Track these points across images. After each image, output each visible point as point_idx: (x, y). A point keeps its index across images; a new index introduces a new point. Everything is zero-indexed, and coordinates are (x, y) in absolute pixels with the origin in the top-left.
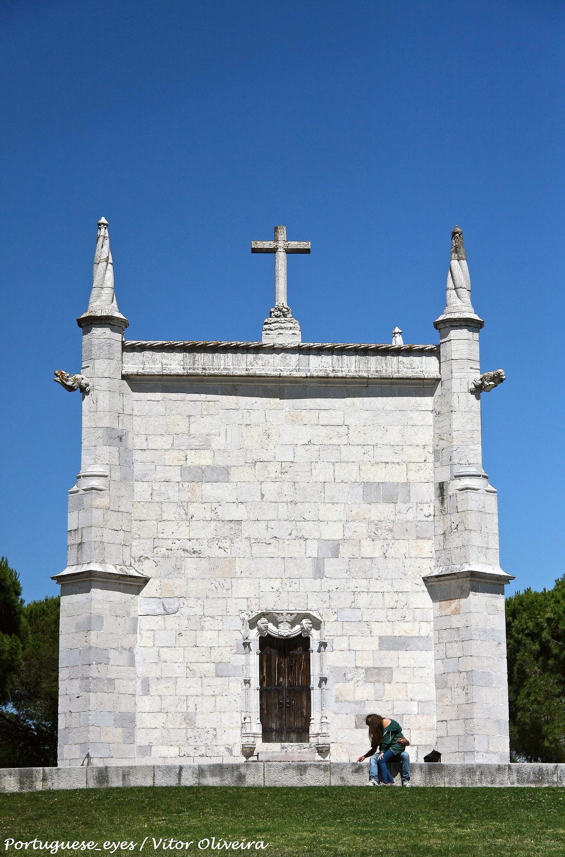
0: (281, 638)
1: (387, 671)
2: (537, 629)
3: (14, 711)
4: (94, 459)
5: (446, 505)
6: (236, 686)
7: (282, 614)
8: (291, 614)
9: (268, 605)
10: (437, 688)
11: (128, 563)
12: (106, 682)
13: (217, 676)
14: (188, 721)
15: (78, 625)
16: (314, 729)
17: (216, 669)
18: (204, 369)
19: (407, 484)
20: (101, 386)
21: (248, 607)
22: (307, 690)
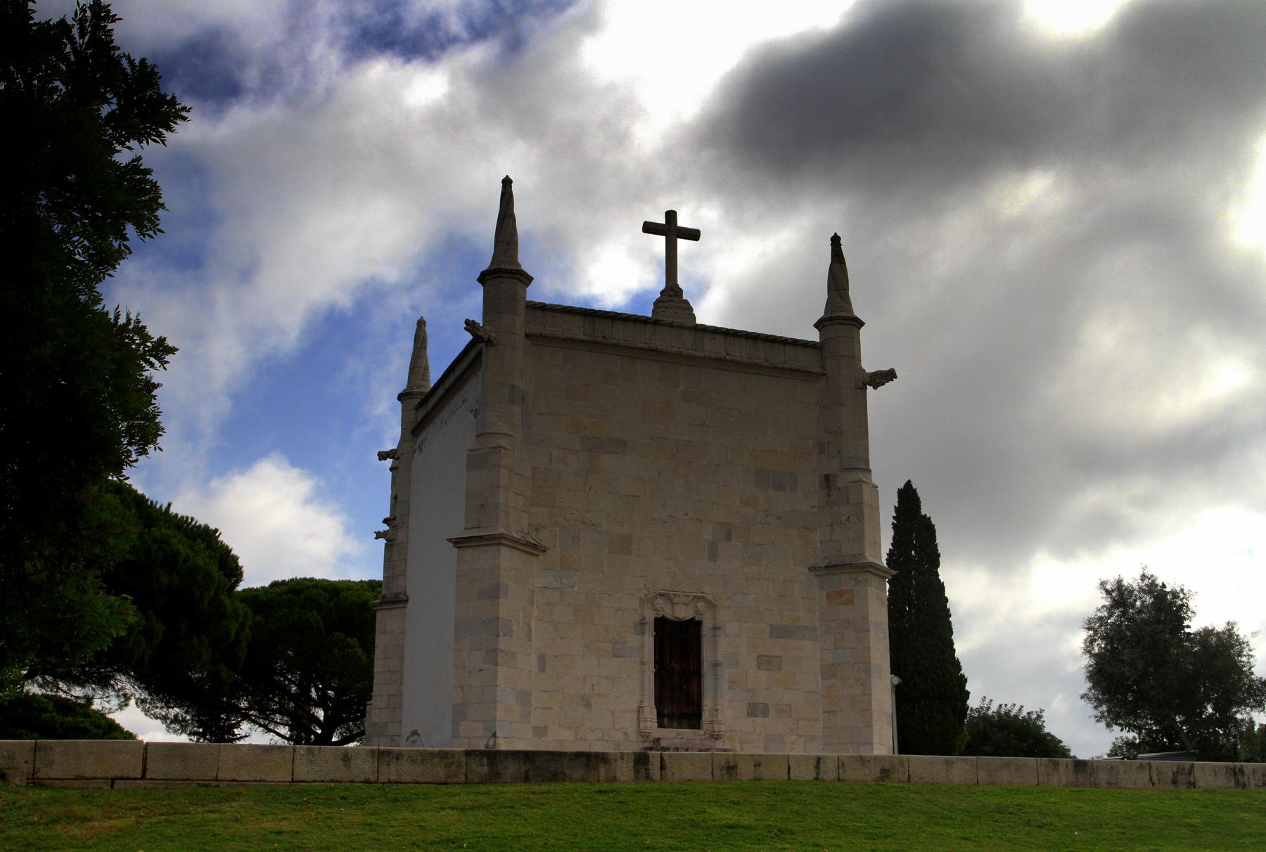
2: (87, 611)
3: (23, 672)
8: (688, 596)
10: (823, 679)
11: (526, 531)
13: (615, 656)
14: (585, 702)
16: (706, 716)
18: (604, 337)
21: (645, 586)
22: (698, 674)
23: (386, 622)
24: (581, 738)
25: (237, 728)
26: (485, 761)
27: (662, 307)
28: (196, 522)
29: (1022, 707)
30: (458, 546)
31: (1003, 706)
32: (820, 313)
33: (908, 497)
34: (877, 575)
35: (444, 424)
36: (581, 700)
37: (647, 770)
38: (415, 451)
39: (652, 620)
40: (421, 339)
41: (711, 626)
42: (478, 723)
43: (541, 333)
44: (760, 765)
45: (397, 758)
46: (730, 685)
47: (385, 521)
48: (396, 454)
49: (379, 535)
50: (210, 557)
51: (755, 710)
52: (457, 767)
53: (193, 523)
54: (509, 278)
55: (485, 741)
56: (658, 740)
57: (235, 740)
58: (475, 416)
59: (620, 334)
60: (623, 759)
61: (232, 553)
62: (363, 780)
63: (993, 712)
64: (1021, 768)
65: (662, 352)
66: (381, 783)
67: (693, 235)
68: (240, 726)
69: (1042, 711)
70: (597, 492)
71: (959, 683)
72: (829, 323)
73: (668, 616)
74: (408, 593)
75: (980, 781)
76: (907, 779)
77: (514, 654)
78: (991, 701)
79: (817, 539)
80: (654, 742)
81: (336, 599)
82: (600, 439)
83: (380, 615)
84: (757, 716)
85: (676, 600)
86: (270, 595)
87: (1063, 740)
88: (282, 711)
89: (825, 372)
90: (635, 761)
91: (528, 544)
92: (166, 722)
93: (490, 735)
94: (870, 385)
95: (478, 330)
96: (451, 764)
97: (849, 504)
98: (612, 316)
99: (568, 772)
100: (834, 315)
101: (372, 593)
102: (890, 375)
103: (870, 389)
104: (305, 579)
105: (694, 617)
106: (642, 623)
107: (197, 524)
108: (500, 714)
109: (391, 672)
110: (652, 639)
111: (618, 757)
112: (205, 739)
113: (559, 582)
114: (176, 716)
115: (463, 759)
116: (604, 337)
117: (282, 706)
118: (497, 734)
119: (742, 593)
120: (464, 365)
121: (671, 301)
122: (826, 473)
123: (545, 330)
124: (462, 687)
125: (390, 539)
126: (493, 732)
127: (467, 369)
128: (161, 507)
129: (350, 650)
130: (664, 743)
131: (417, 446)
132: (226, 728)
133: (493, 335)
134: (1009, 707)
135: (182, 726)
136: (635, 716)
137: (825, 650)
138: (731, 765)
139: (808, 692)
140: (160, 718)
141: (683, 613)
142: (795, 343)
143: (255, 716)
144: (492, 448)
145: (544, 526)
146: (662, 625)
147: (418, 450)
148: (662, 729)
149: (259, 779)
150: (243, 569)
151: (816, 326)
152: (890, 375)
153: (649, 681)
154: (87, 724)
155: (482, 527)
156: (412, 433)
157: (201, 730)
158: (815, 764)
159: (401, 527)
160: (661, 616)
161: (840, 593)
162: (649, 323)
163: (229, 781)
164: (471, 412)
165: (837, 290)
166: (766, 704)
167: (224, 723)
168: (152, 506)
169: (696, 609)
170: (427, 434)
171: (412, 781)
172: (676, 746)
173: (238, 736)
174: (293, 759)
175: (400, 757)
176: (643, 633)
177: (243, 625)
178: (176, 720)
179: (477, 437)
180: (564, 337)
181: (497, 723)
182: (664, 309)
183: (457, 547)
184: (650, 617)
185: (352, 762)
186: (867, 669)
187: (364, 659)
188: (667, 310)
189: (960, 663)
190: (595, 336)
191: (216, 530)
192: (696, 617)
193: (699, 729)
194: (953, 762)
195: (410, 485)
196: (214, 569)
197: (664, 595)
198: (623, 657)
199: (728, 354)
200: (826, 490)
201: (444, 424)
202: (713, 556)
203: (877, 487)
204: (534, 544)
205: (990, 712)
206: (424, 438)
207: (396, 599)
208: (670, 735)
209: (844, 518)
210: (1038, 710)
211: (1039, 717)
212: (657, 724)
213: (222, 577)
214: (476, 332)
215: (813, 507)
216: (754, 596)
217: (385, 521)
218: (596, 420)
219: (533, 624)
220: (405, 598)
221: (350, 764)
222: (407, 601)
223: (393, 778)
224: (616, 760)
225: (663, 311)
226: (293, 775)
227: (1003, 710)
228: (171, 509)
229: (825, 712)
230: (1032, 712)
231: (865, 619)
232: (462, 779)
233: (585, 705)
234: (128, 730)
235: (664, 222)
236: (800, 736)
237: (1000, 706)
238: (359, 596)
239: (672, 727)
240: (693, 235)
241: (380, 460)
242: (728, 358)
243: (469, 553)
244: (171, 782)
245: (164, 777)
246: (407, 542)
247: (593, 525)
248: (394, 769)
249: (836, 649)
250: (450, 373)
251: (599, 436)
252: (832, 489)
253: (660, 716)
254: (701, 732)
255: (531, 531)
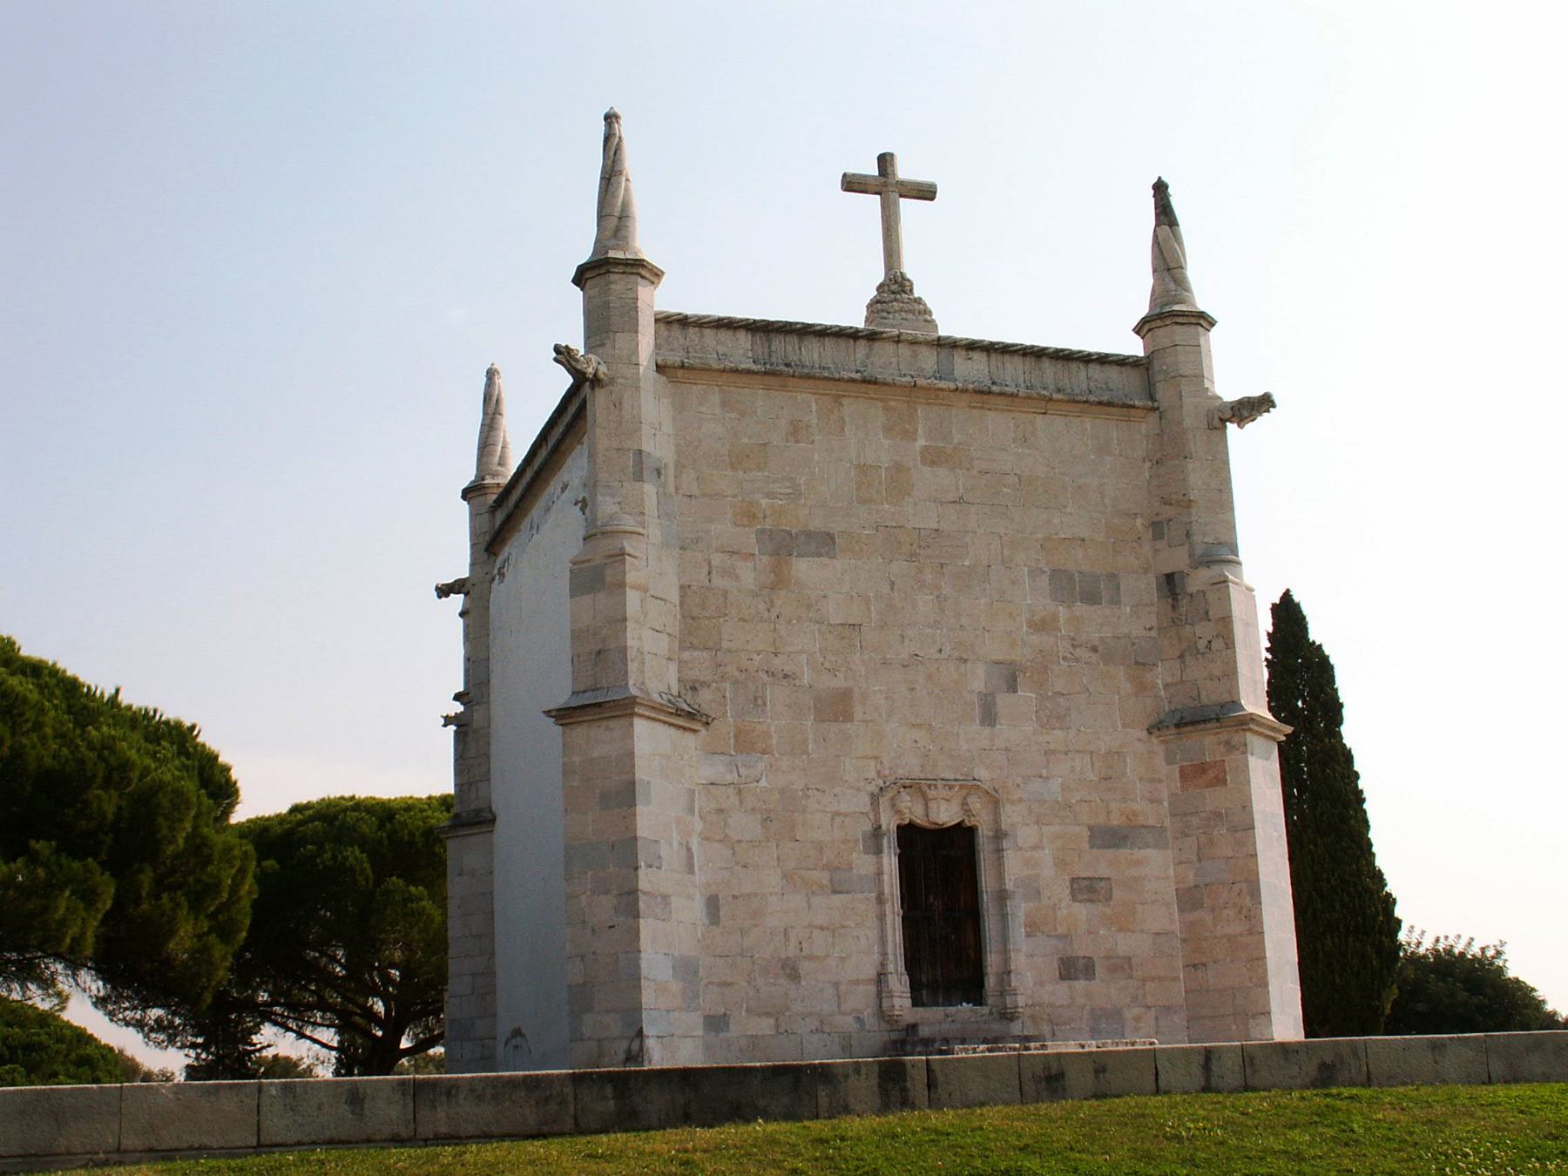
0: (936, 827)
1: (1103, 884)
4: (619, 503)
5: (1183, 610)
6: (863, 904)
7: (935, 785)
9: (911, 767)
10: (1181, 910)
12: (659, 899)
13: (835, 892)
15: (85, 909)
16: (991, 982)
17: (831, 880)
18: (787, 365)
19: (1113, 577)
20: (627, 379)
21: (878, 772)
23: (460, 854)
24: (786, 1031)
25: (256, 1033)
26: (609, 1091)
27: (883, 311)
28: (161, 716)
29: (1472, 939)
30: (561, 722)
31: (1442, 940)
32: (1143, 310)
33: (1288, 614)
34: (1261, 734)
35: (534, 531)
36: (783, 968)
37: (904, 1090)
38: (493, 579)
39: (893, 828)
40: (495, 399)
41: (990, 834)
42: (613, 1014)
43: (683, 362)
44: (1104, 1071)
45: (449, 1094)
46: (1028, 929)
47: (458, 697)
48: (463, 586)
49: (448, 721)
50: (185, 767)
51: (1071, 969)
52: (560, 1104)
53: (157, 718)
54: (624, 273)
55: (625, 1044)
56: (913, 1027)
57: (254, 1052)
58: (583, 510)
59: (813, 353)
60: (859, 1075)
61: (220, 759)
62: (390, 1137)
63: (1427, 950)
64: (1563, 1049)
65: (885, 384)
66: (422, 1140)
67: (926, 193)
68: (260, 1029)
69: (1503, 944)
70: (789, 622)
71: (385, 898)
72: (1159, 323)
73: (919, 821)
74: (494, 808)
75: (1493, 1076)
76: (1366, 1080)
77: (665, 897)
78: (1423, 932)
79: (1159, 681)
80: (907, 1030)
81: (388, 825)
82: (789, 533)
83: (450, 844)
84: (1076, 979)
85: (932, 793)
86: (289, 826)
87: (1537, 988)
88: (324, 1006)
89: (1156, 404)
90: (880, 1076)
91: (679, 713)
92: (143, 1030)
93: (634, 1034)
94: (1231, 422)
95: (577, 361)
96: (548, 1098)
97: (1209, 620)
98: (799, 330)
99: (761, 1103)
100: (1167, 309)
101: (445, 813)
102: (1261, 404)
103: (1231, 428)
104: (342, 798)
105: (963, 820)
106: (877, 833)
107: (163, 719)
108: (647, 998)
109: (475, 936)
110: (895, 860)
111: (850, 1071)
112: (208, 1053)
113: (735, 774)
114: (158, 1020)
115: (568, 1090)
116: (787, 365)
117: (321, 999)
118: (645, 1031)
119: (1041, 777)
120: (560, 428)
121: (896, 300)
122: (1169, 571)
123: (687, 358)
124: (583, 957)
125: (462, 723)
126: (637, 1029)
127: (564, 435)
128: (102, 694)
129: (414, 905)
130: (924, 1032)
131: (496, 571)
132: (239, 1035)
133: (603, 369)
134: (1451, 941)
135: (169, 1036)
136: (872, 989)
137: (1181, 863)
138: (1054, 1072)
139: (1158, 934)
140: (134, 1026)
141: (946, 814)
142: (1103, 360)
143: (282, 1015)
144: (611, 556)
145: (704, 682)
146: (909, 835)
147: (497, 577)
148: (921, 1009)
149: (196, 1145)
150: (238, 784)
151: (1138, 330)
152: (1261, 404)
153: (894, 934)
154: (44, 1038)
155: (602, 688)
156: (486, 550)
157: (200, 1040)
158: (1202, 1063)
159: (477, 704)
160: (907, 822)
161: (1202, 769)
162: (863, 337)
163: (141, 1152)
164: (576, 504)
165: (1169, 270)
166: (1090, 958)
167: (236, 1027)
168: (90, 695)
169: (966, 807)
170: (510, 549)
171: (478, 1133)
172: (946, 1036)
173: (259, 1046)
174: (258, 1106)
175: (453, 1092)
176: (878, 851)
177: (242, 872)
178: (159, 1026)
179: (585, 539)
180: (722, 366)
181: (644, 1014)
182: (885, 314)
183: (561, 725)
184: (889, 823)
185: (366, 1106)
186: (1255, 893)
187: (438, 919)
188: (891, 316)
189: (1382, 875)
190: (772, 364)
191: (193, 727)
192: (966, 821)
193: (981, 1004)
194: (1444, 1045)
195: (488, 635)
196: (190, 786)
197: (910, 787)
198: (848, 892)
199: (994, 383)
200: (1170, 600)
201: (534, 531)
202: (989, 716)
203: (1251, 590)
204: (689, 712)
205: (1422, 951)
206: (505, 557)
207: (478, 820)
208: (933, 1019)
209: (1202, 644)
210: (1497, 943)
211: (1499, 953)
212: (910, 1000)
213: (205, 799)
214: (574, 363)
215: (1150, 629)
216: (1060, 780)
217: (458, 697)
218: (780, 502)
219: (695, 848)
220: (489, 816)
221: (362, 1109)
222: (493, 820)
223: (443, 1129)
224: (846, 1076)
225: (885, 318)
226: (259, 1136)
227: (1441, 947)
228: (120, 697)
229: (1188, 966)
230: (1488, 947)
231: (1246, 807)
232: (569, 1123)
233: (789, 976)
234: (107, 1042)
235: (877, 174)
236: (1149, 1007)
237: (1437, 940)
238: (424, 820)
239: (937, 1005)
240: (926, 193)
241: (440, 597)
242: (994, 388)
243: (580, 733)
244: (34, 1159)
245: (21, 1152)
246: (489, 726)
247: (786, 676)
248: (444, 1114)
249: (1200, 860)
250: (541, 446)
251: (788, 528)
252: (1180, 597)
253: (915, 987)
254: (985, 1010)
255: (683, 692)
